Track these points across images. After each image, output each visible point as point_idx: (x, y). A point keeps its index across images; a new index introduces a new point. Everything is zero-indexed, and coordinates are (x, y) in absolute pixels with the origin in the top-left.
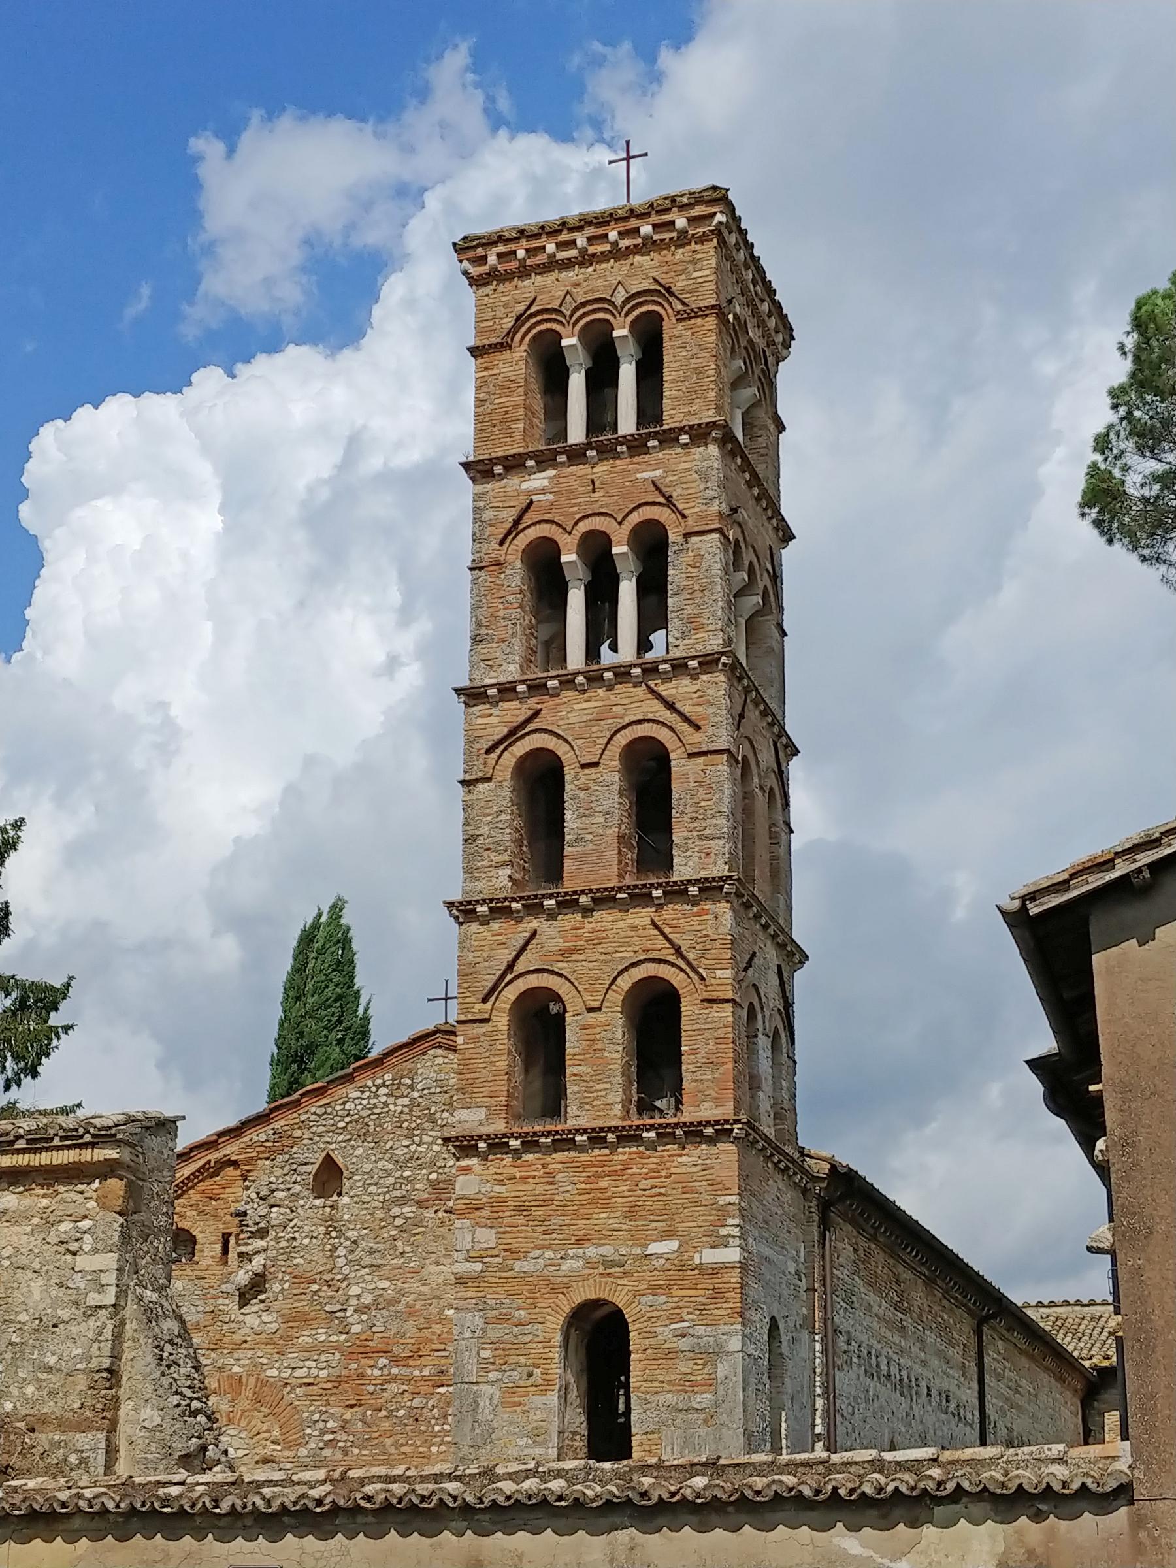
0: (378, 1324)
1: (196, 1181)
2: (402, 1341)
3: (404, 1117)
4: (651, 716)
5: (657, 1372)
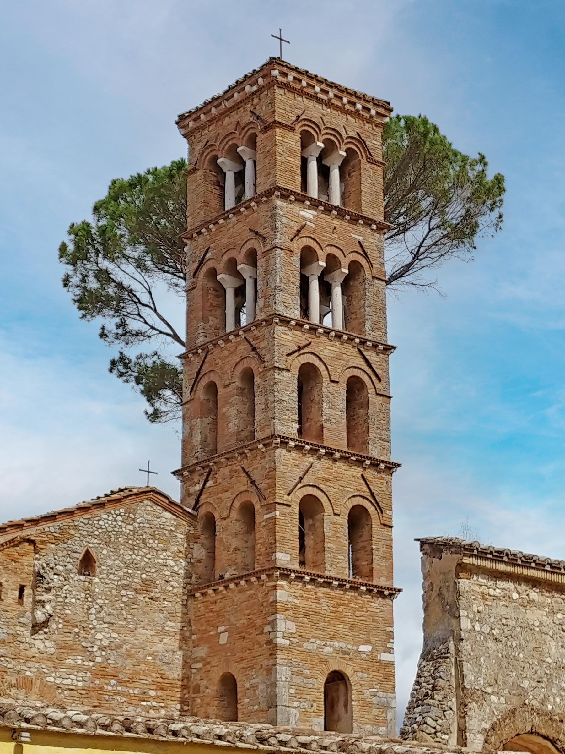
0: (111, 658)
2: (124, 671)
3: (130, 537)
4: (360, 366)
5: (365, 713)
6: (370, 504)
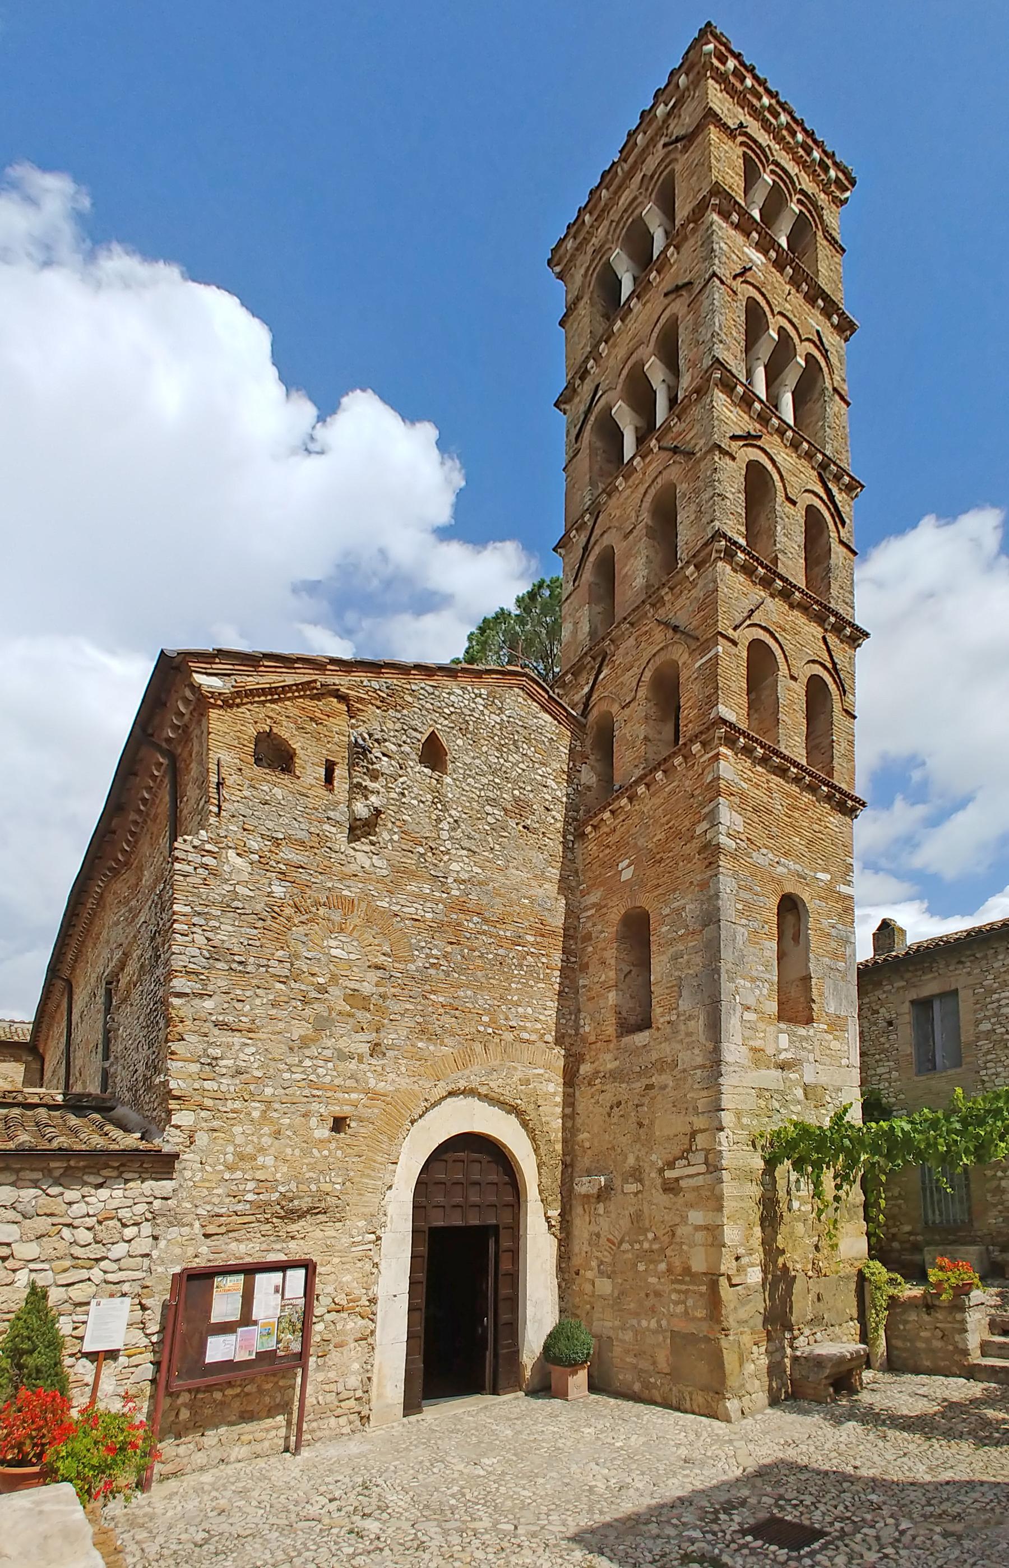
1: (296, 694)
6: (831, 679)
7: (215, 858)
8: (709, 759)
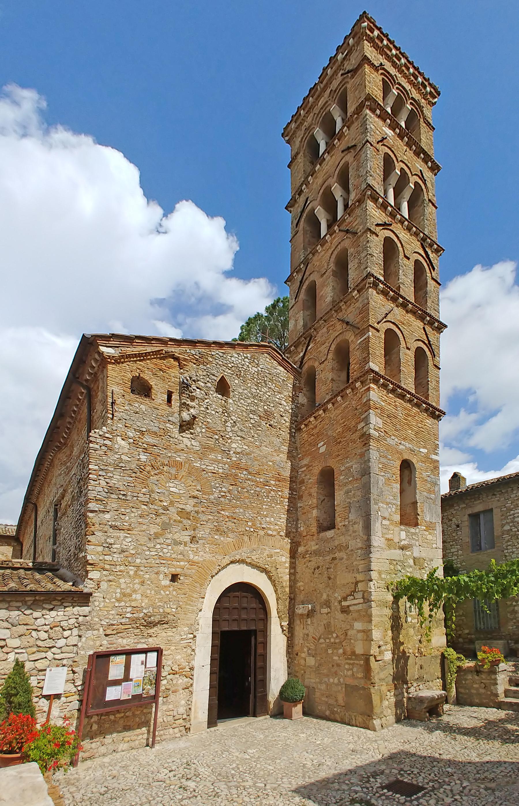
1: (152, 357)
6: (427, 349)
7: (111, 441)
8: (365, 390)
